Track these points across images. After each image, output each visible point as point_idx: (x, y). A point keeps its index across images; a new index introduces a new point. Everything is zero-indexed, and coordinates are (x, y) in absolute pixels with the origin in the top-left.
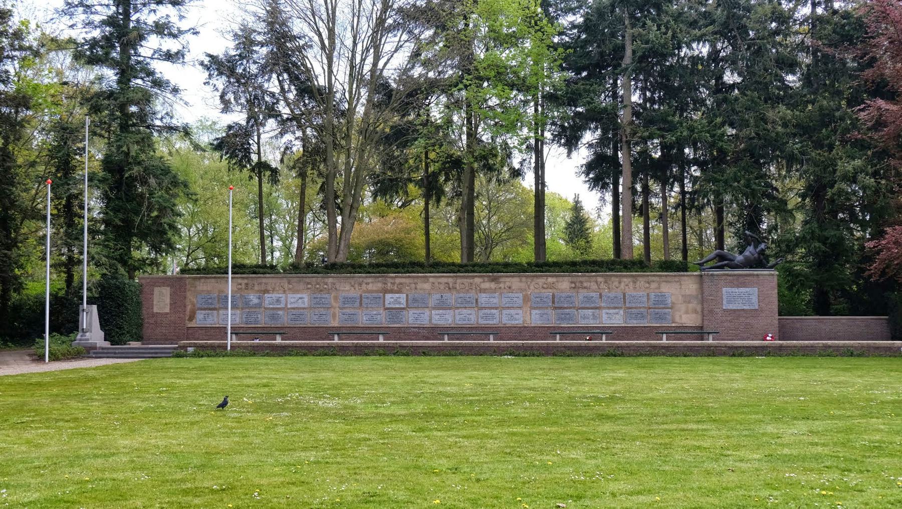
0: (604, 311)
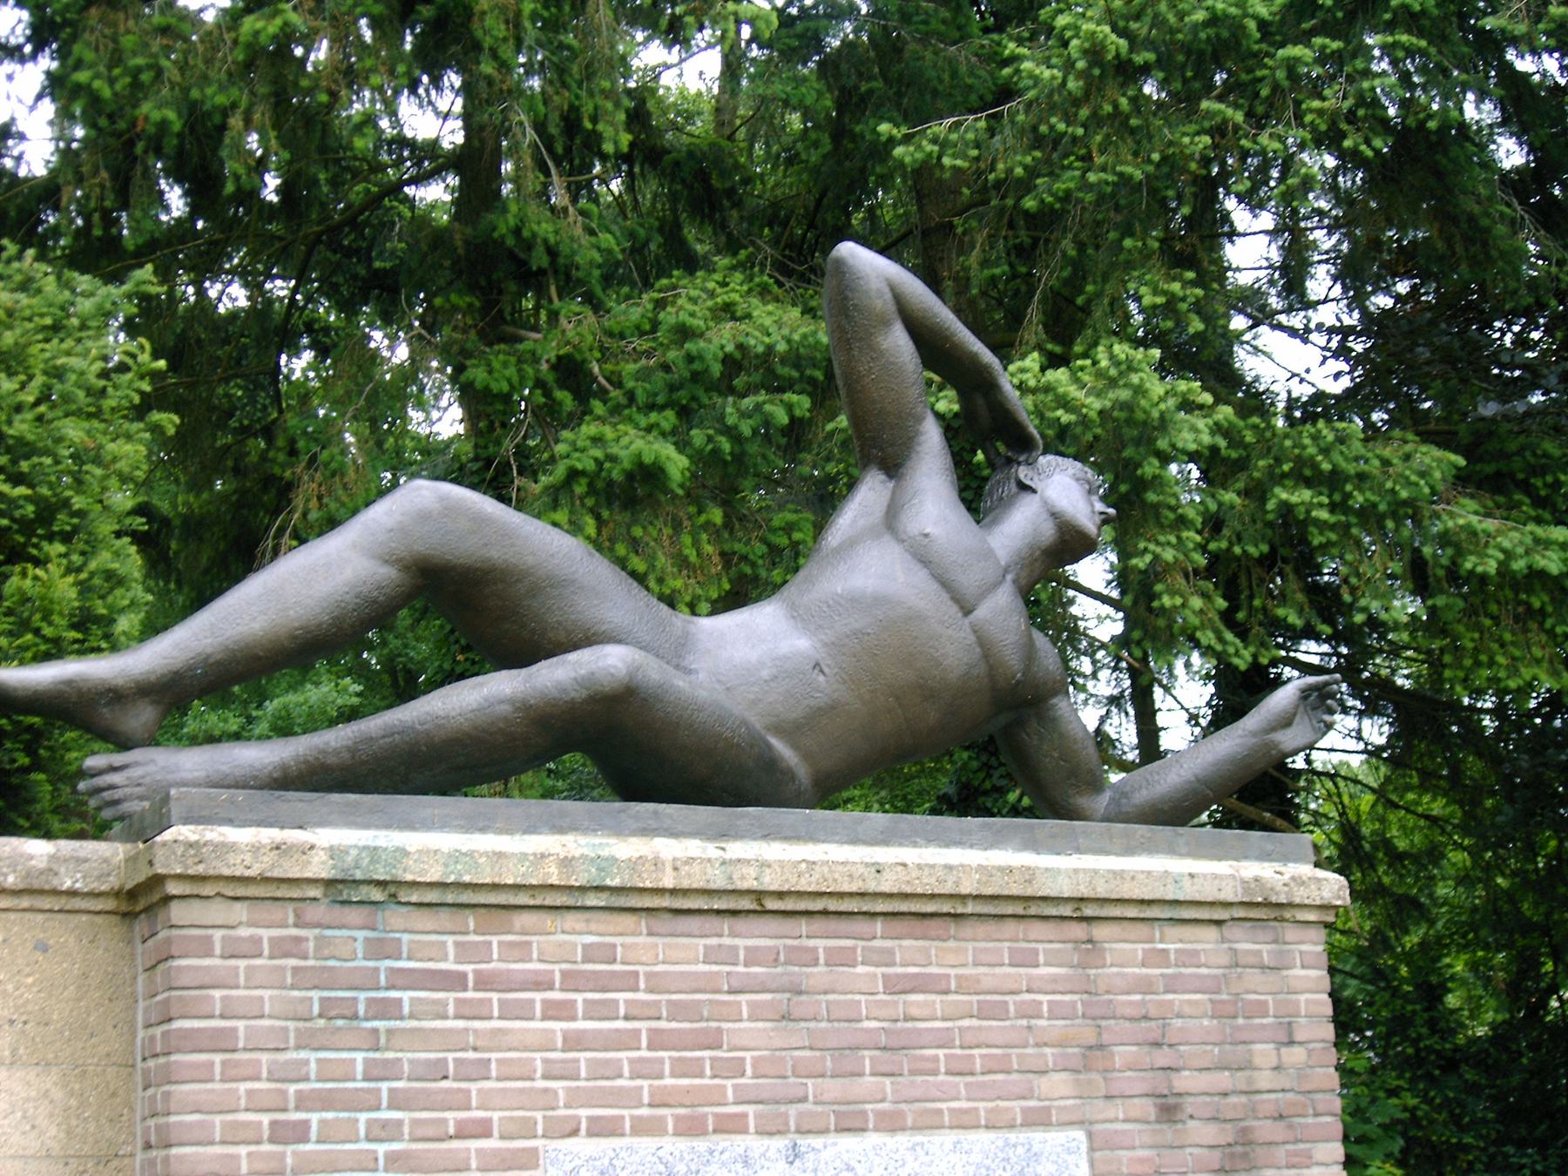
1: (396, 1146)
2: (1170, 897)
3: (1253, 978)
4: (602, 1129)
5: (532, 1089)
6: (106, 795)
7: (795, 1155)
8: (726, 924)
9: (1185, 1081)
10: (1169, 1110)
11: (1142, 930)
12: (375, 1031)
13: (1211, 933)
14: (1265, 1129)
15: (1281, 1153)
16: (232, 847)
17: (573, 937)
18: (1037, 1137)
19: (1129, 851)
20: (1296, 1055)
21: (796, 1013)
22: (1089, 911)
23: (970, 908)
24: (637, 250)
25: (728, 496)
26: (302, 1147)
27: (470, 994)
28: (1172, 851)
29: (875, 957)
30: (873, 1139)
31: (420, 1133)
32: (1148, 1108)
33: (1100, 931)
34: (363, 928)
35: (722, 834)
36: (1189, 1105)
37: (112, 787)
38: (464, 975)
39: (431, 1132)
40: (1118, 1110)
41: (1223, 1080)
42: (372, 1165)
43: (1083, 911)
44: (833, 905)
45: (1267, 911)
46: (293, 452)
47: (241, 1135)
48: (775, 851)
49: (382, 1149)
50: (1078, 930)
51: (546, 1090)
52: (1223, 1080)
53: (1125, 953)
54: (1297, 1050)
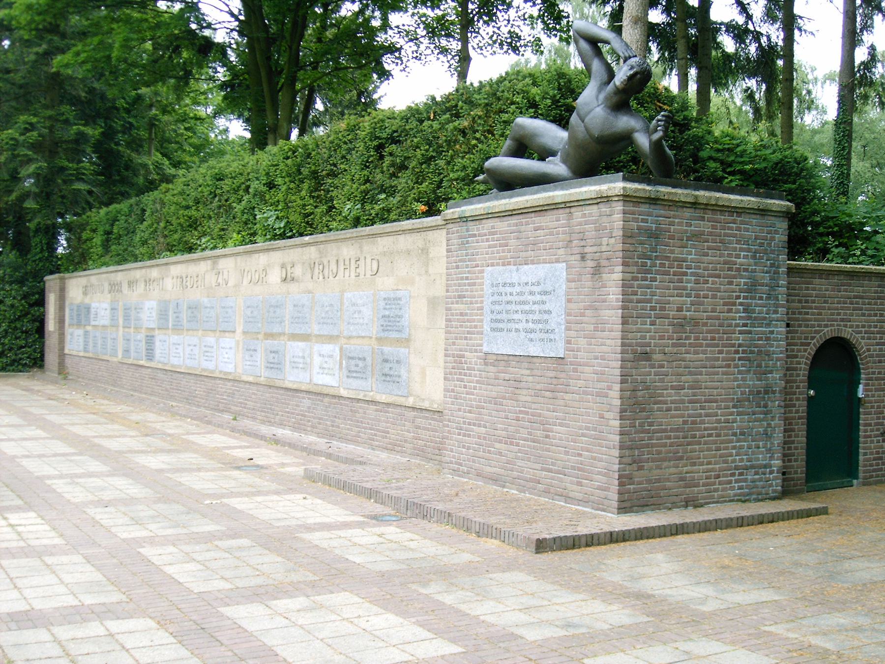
0: (317, 347)
3: (605, 219)
4: (493, 265)
6: (268, 106)
7: (518, 270)
8: (510, 218)
9: (588, 249)
10: (583, 258)
11: (580, 208)
13: (595, 207)
14: (604, 263)
15: (606, 270)
16: (557, 196)
17: (488, 224)
18: (557, 265)
19: (581, 186)
20: (612, 241)
28: (591, 185)
30: (530, 266)
32: (578, 257)
33: (573, 210)
35: (511, 197)
36: (588, 256)
40: (573, 258)
41: (595, 249)
43: (567, 205)
45: (604, 199)
48: (578, 190)
50: (567, 210)
52: (595, 249)
53: (577, 213)
54: (613, 239)
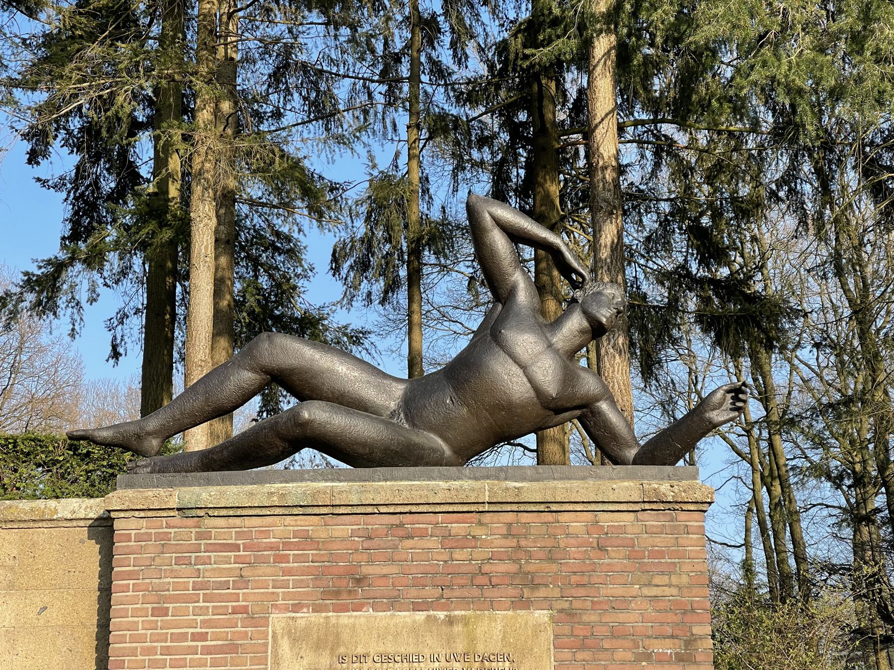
1: (206, 617)
2: (600, 500)
5: (267, 593)
12: (199, 569)
21: (396, 558)
22: (554, 507)
23: (487, 507)
24: (714, 52)
25: (843, 187)
26: (165, 618)
27: (241, 553)
29: (211, 548)
31: (216, 612)
34: (194, 528)
37: (728, 336)
38: (239, 545)
39: (221, 611)
42: (195, 625)
44: (414, 509)
46: (763, 90)
47: (139, 614)
49: (199, 618)
50: (549, 517)
51: (273, 593)
